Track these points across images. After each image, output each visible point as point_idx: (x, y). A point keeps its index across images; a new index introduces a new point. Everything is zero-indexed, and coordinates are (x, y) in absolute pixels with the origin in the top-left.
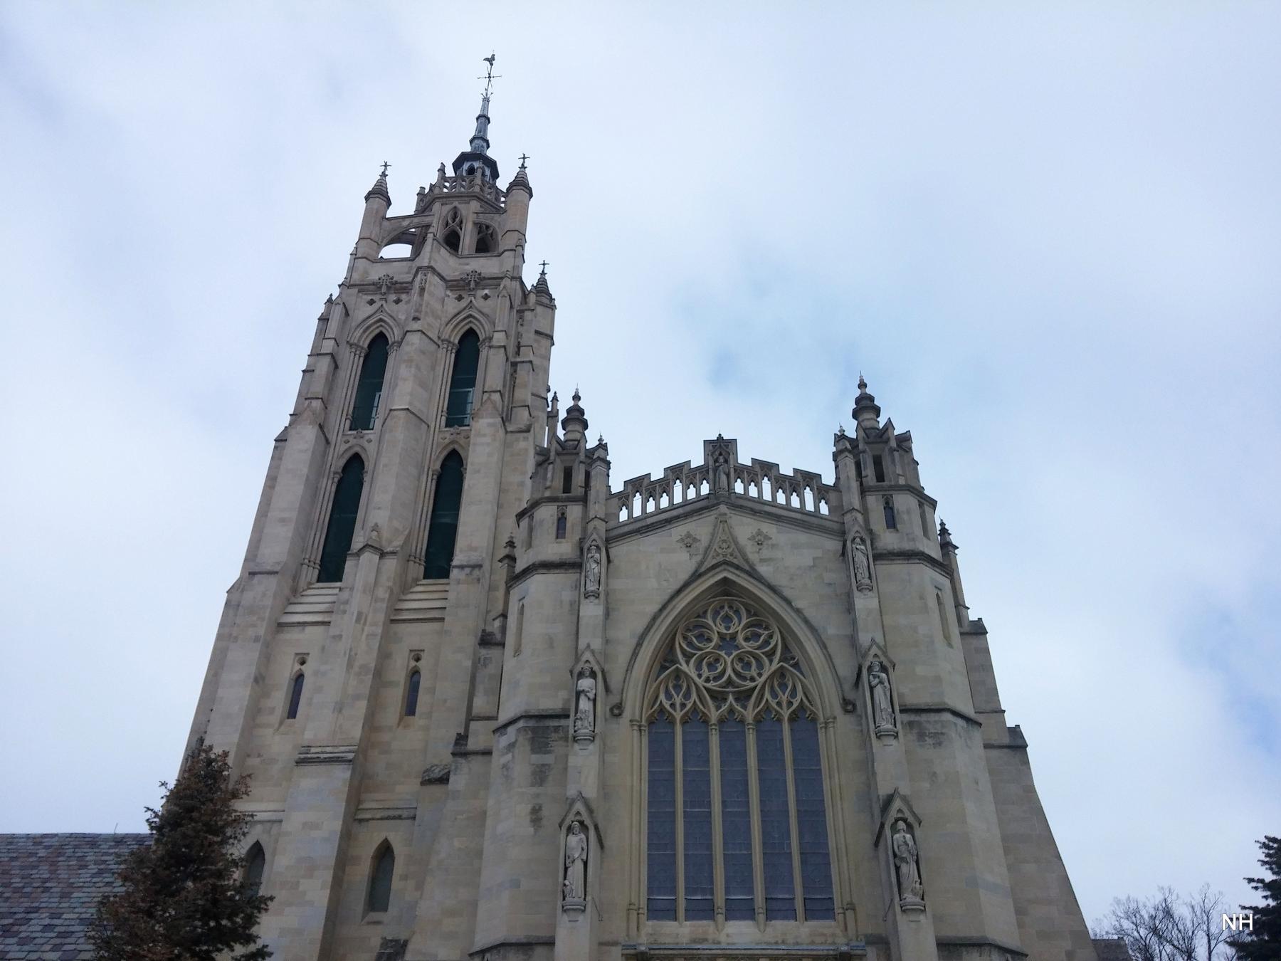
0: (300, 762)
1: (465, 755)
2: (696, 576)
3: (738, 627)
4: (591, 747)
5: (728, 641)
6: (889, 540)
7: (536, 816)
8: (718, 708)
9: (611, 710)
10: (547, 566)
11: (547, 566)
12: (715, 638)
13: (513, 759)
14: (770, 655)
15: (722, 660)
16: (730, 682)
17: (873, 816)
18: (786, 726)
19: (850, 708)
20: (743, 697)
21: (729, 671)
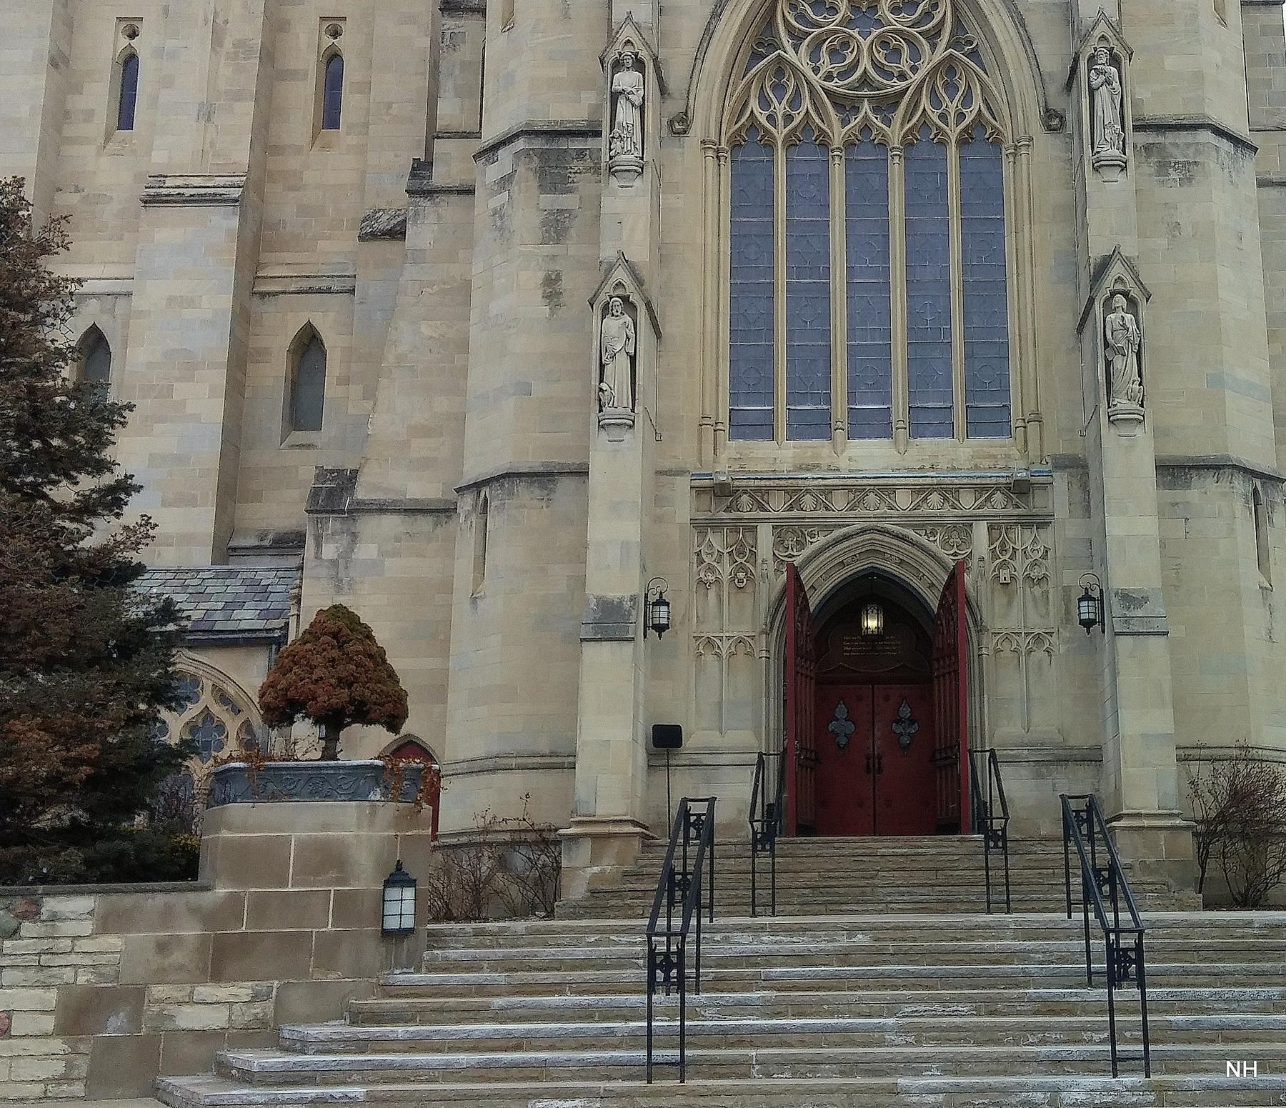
0: (149, 201)
1: (430, 193)
4: (638, 182)
7: (552, 289)
8: (844, 122)
14: (933, 37)
15: (853, 44)
16: (865, 81)
17: (1077, 288)
18: (952, 152)
19: (1055, 122)
20: (886, 105)
21: (865, 63)
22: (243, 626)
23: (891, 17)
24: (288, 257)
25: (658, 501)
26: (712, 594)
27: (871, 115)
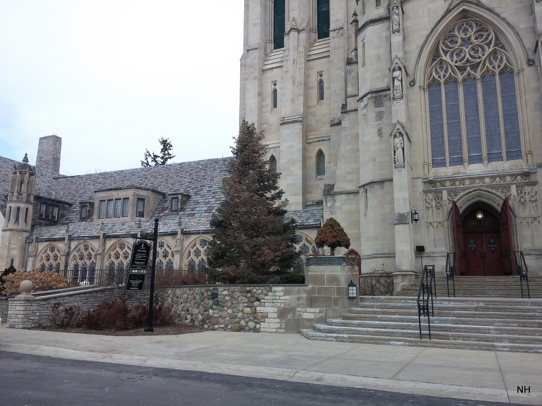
1: (347, 112)
2: (448, 11)
3: (471, 33)
4: (402, 101)
5: (466, 41)
7: (380, 133)
8: (462, 74)
9: (410, 83)
10: (373, 22)
11: (373, 22)
12: (460, 41)
13: (368, 112)
14: (489, 45)
16: (468, 61)
19: (531, 63)
20: (475, 67)
22: (311, 224)
23: (475, 41)
24: (314, 133)
25: (413, 186)
26: (430, 210)
27: (470, 71)
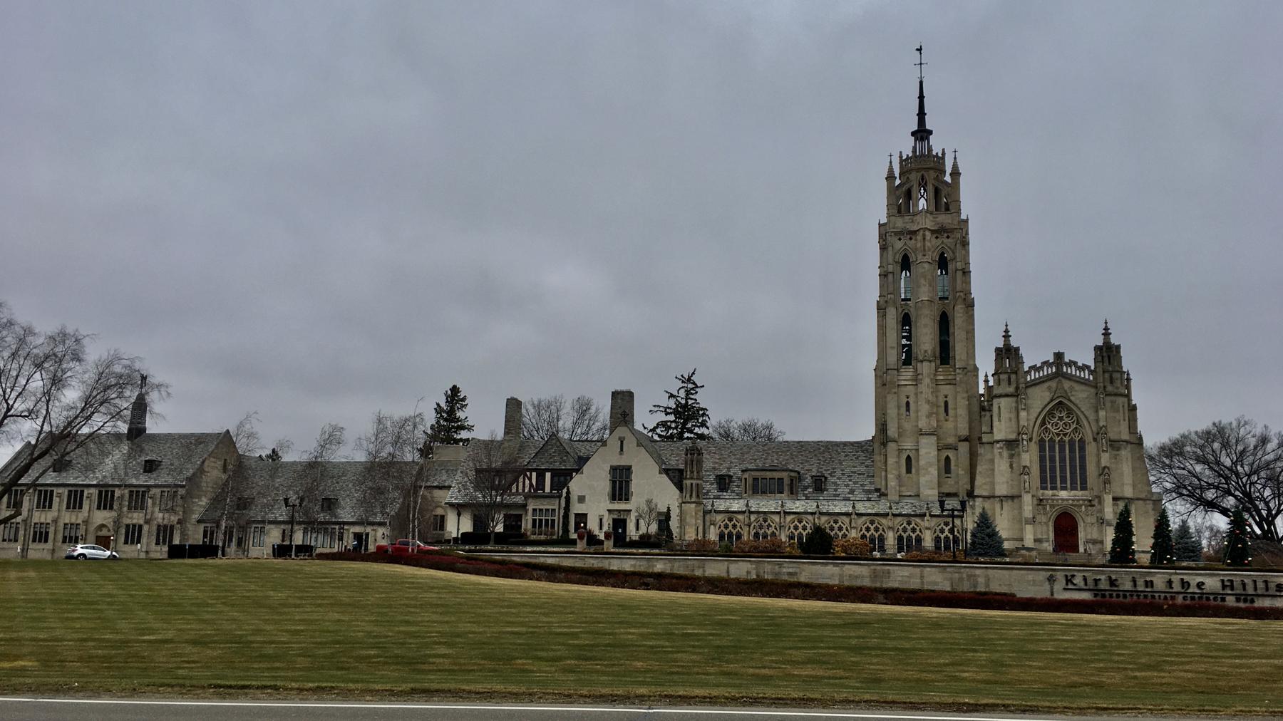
6: (1110, 388)
